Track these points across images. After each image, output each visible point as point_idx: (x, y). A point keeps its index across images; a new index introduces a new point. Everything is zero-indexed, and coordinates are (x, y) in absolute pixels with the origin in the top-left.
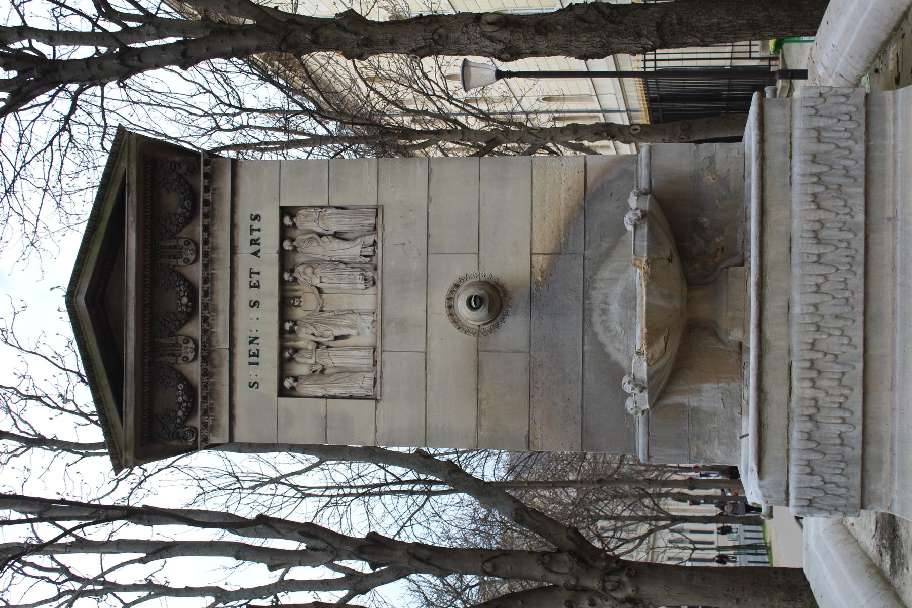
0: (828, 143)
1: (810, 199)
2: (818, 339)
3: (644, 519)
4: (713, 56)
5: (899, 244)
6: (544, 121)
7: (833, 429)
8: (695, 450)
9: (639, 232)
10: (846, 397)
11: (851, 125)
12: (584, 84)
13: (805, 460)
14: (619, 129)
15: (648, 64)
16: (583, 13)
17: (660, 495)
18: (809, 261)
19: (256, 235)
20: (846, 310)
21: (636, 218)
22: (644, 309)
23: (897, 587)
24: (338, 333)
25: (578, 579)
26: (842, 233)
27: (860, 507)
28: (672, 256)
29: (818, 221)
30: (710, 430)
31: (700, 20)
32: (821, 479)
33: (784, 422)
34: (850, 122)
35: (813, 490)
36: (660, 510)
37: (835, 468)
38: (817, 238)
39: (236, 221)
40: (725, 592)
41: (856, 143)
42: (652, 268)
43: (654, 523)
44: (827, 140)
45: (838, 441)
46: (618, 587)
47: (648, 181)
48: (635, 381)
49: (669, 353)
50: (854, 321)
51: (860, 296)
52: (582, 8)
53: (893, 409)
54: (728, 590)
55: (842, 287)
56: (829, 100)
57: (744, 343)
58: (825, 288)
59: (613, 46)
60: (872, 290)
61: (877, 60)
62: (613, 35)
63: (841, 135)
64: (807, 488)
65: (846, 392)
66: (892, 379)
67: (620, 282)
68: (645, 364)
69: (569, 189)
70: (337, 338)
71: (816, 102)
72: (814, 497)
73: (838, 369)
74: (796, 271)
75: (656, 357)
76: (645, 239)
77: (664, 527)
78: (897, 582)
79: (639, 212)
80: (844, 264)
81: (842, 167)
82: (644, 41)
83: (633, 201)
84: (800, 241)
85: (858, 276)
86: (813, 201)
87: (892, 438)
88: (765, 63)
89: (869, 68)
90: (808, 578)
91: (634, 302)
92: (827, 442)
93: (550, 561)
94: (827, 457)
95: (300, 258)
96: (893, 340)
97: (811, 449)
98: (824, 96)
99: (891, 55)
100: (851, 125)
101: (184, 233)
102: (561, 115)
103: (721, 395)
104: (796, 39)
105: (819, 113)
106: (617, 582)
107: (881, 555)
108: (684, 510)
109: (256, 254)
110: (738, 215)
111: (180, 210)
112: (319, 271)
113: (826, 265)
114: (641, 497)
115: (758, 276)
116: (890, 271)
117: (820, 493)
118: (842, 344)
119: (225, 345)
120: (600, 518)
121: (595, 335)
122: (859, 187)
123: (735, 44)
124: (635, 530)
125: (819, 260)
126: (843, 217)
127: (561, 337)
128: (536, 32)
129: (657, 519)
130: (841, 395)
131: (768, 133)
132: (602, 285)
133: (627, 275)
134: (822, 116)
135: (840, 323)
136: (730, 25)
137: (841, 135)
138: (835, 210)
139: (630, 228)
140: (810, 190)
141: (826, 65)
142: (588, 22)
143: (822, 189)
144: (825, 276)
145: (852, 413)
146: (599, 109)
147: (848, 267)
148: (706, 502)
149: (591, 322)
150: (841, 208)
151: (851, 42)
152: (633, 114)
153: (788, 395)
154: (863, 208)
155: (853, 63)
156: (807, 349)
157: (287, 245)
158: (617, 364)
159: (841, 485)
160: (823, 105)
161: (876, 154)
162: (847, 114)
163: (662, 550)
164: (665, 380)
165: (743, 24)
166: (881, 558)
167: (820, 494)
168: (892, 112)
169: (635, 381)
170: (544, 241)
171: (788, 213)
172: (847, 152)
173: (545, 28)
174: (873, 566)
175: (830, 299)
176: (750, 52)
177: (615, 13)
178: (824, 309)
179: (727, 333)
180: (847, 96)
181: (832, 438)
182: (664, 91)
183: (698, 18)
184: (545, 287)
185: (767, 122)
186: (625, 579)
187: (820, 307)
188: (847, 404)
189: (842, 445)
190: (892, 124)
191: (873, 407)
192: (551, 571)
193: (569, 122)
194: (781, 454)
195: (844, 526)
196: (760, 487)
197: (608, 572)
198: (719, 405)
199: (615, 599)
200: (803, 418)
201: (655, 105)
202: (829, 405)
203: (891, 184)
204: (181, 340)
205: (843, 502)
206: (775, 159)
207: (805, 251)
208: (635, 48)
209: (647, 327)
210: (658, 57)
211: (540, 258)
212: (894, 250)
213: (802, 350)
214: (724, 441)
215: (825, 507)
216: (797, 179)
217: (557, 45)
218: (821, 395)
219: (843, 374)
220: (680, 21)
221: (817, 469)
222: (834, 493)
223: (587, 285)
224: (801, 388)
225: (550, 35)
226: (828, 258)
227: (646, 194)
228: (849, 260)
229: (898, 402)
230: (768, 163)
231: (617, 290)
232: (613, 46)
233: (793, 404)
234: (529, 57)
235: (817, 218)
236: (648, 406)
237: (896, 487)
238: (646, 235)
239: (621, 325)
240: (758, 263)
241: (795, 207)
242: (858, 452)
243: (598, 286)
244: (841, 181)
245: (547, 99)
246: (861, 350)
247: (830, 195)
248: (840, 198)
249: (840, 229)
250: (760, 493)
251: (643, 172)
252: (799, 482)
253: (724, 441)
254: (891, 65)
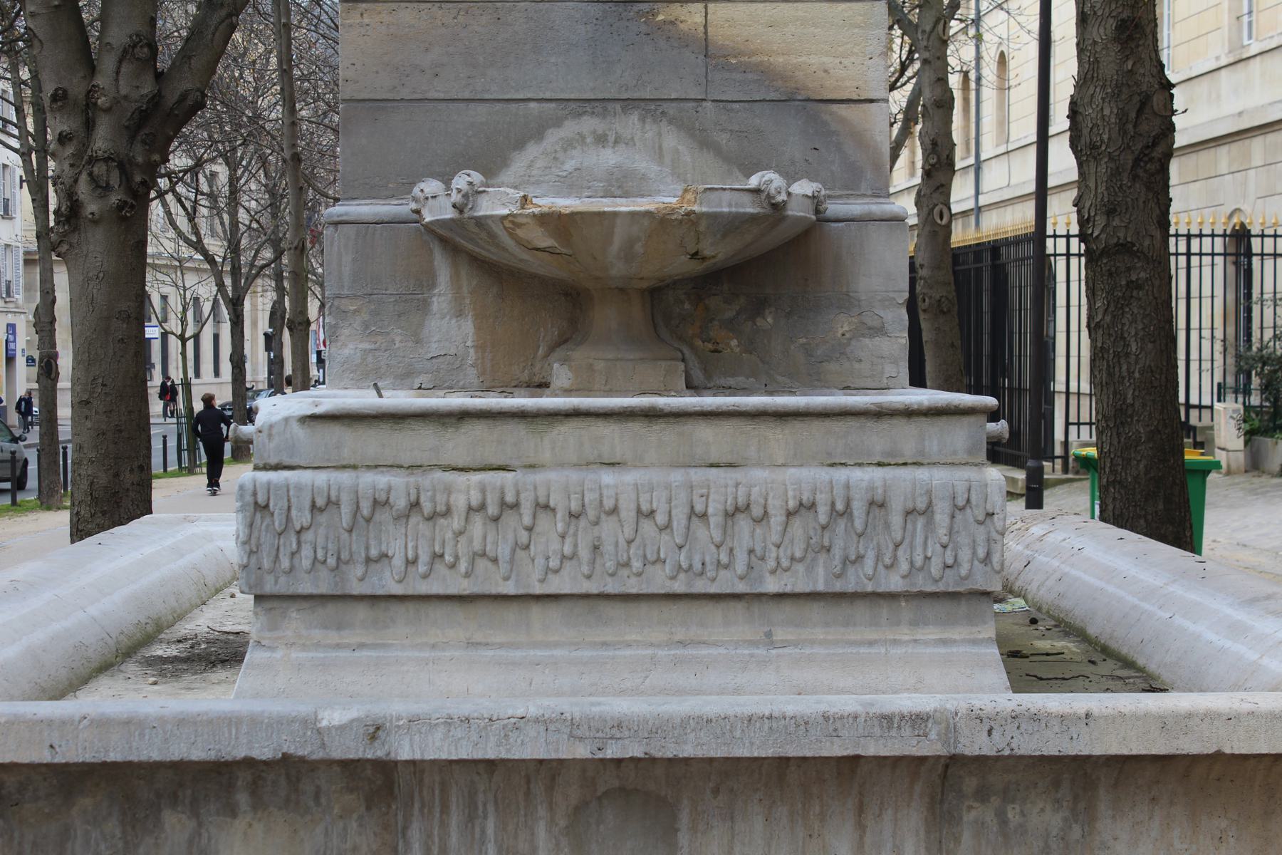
0: (904, 529)
1: (805, 499)
2: (555, 516)
3: (234, 247)
4: (1074, 361)
5: (725, 651)
6: (960, 54)
7: (396, 543)
8: (352, 308)
9: (747, 198)
10: (453, 566)
11: (935, 568)
12: (1026, 130)
13: (338, 497)
14: (942, 185)
15: (1061, 243)
16: (1156, 108)
17: (278, 277)
18: (696, 498)
20: (608, 564)
21: (773, 192)
22: (606, 209)
23: (123, 667)
25: (108, 110)
26: (745, 555)
27: (259, 593)
28: (704, 259)
29: (766, 512)
30: (388, 333)
31: (1134, 321)
32: (305, 524)
33: (406, 459)
34: (941, 566)
35: (285, 512)
36: (251, 279)
37: (325, 549)
38: (733, 513)
40: (100, 380)
41: (904, 577)
42: (681, 222)
43: (227, 268)
44: (909, 526)
45: (374, 553)
46: (98, 186)
47: (841, 215)
48: (473, 194)
49: (525, 256)
50: (589, 577)
51: (633, 587)
52: (1165, 106)
53: (434, 646)
54: (104, 385)
55: (649, 556)
56: (982, 528)
57: (547, 391)
58: (647, 527)
59: (1093, 164)
60: (644, 607)
61: (1053, 623)
62: (1111, 165)
63: (919, 550)
64: (289, 501)
65: (463, 566)
66: (487, 644)
67: (656, 168)
68: (506, 212)
69: (826, 71)
71: (977, 506)
72: (272, 514)
73: (504, 551)
74: (677, 476)
75: (519, 232)
76: (734, 210)
77: (220, 285)
78: (131, 667)
79: (783, 197)
80: (690, 558)
81: (862, 552)
82: (1101, 220)
83: (803, 188)
84: (731, 483)
85: (668, 583)
86: (801, 504)
87: (384, 646)
88: (1058, 450)
89: (1039, 609)
90: (134, 524)
91: (619, 192)
92: (372, 535)
93: (138, 59)
94: (346, 535)
96: (556, 645)
97: (358, 507)
98: (988, 521)
99: (1060, 644)
100: (935, 568)
102: (973, 85)
103: (453, 351)
104: (1097, 494)
105: (957, 511)
106: (108, 184)
107: (179, 641)
108: (254, 324)
110: (780, 378)
113: (688, 528)
114: (275, 243)
115: (667, 409)
116: (678, 637)
117: (280, 525)
118: (547, 558)
120: (232, 165)
121: (558, 123)
122: (826, 583)
123: (1094, 398)
124: (213, 234)
125: (696, 515)
126: (774, 555)
127: (553, 60)
128: (1123, 20)
129: (235, 272)
130: (457, 558)
131: (924, 423)
132: (649, 135)
133: (669, 180)
134: (953, 517)
135: (584, 553)
136: (1125, 374)
137: (919, 550)
138: (786, 541)
139: (754, 181)
140: (822, 499)
141: (1046, 539)
142: (1137, 117)
143: (823, 518)
144: (668, 527)
145: (425, 576)
146: (983, 157)
147: (685, 565)
148: (271, 362)
149: (580, 115)
150: (789, 553)
151: (1086, 578)
152: (973, 219)
153: (454, 465)
154: (788, 589)
155: (1049, 583)
156: (537, 498)
158: (504, 163)
159: (296, 561)
160: (972, 520)
161: (884, 610)
162: (956, 560)
163: (180, 283)
164: (477, 250)
165: (1125, 399)
166: (174, 642)
167: (278, 523)
168: (956, 637)
169: (473, 194)
171: (780, 461)
172: (887, 561)
173: (1130, 38)
174: (160, 628)
175: (626, 536)
176: (1079, 424)
177: (1152, 167)
178: (608, 525)
179: (565, 361)
180: (987, 559)
181: (380, 543)
182: (1012, 270)
183: (1139, 318)
184: (644, 28)
185: (943, 422)
186: (114, 199)
187: (614, 518)
188: (440, 568)
189: (368, 560)
190: (938, 637)
191: (438, 612)
192: (120, 62)
193: (957, 95)
194: (347, 456)
195: (230, 583)
196: (287, 420)
197: (124, 167)
198: (434, 349)
199: (76, 181)
200: (413, 492)
201: (987, 257)
202: (438, 538)
203: (830, 637)
205: (266, 564)
206: (877, 438)
207: (712, 490)
208: (1087, 205)
209: (573, 214)
210: (1074, 261)
211: (699, 19)
212: (715, 644)
213: (535, 488)
214: (370, 359)
215: (255, 534)
216: (841, 475)
217: (1097, 61)
218: (456, 522)
219: (495, 561)
220: (1134, 285)
221: (322, 518)
222: (282, 549)
223: (649, 107)
224: (467, 487)
225: (1117, 47)
227: (817, 212)
228: (697, 566)
229: (447, 654)
230: (870, 424)
231: (642, 163)
232: (1093, 164)
233: (438, 475)
234: (1077, 8)
235: (771, 511)
236: (428, 218)
237: (296, 654)
238: (742, 210)
239: (577, 169)
240: (691, 409)
241: (792, 473)
242: (357, 589)
243: (647, 127)
244: (837, 552)
245: (1002, 60)
246: (538, 590)
247: (812, 533)
248: (806, 550)
249: (751, 551)
250: (275, 418)
251: (856, 207)
252: (299, 488)
253: (370, 359)
254: (1044, 645)
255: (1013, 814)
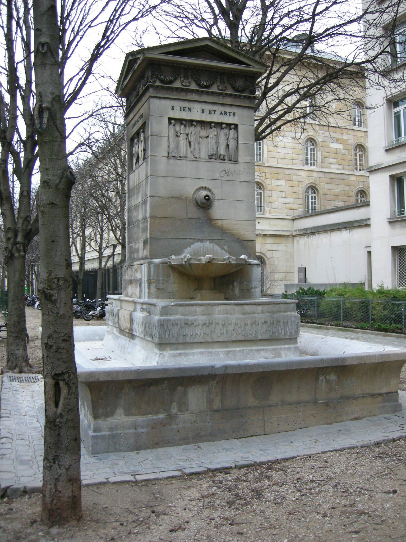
19: (228, 114)
24: (192, 143)
39: (233, 107)
58: (237, 327)
70: (190, 142)
95: (219, 130)
101: (229, 86)
109: (221, 113)
111: (237, 85)
112: (215, 138)
119: (188, 98)
121: (193, 243)
135: (225, 333)
144: (241, 327)
157: (224, 126)
170: (227, 224)
178: (230, 327)
204: (190, 80)
205: (163, 337)
216: (186, 318)
218: (200, 327)
226: (247, 328)
255: (328, 377)
